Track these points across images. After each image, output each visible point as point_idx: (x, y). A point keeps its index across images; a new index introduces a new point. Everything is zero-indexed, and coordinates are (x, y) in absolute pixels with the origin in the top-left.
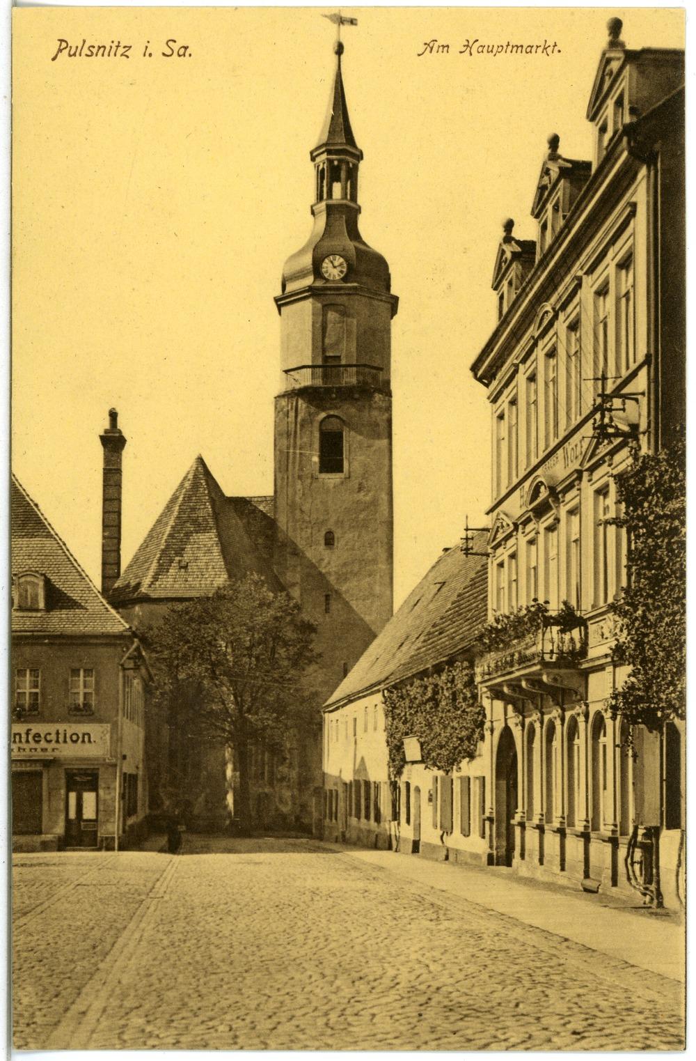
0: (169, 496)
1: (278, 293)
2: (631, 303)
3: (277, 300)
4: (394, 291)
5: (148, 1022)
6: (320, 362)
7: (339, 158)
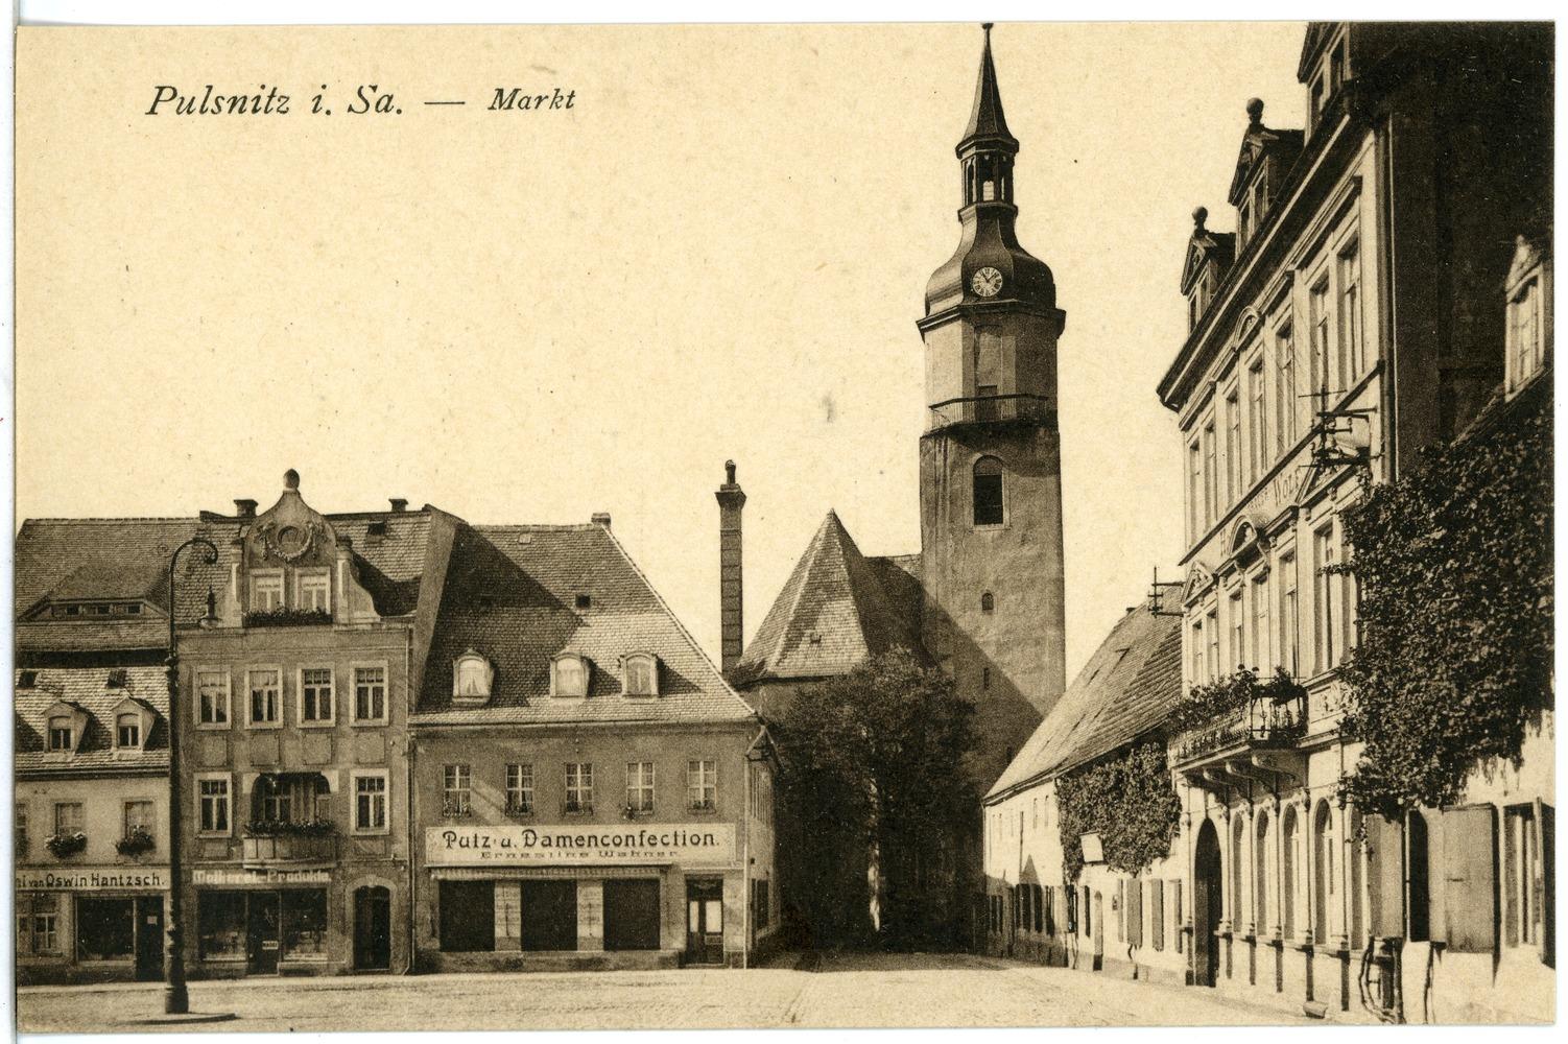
1: (922, 315)
3: (920, 324)
7: (991, 151)
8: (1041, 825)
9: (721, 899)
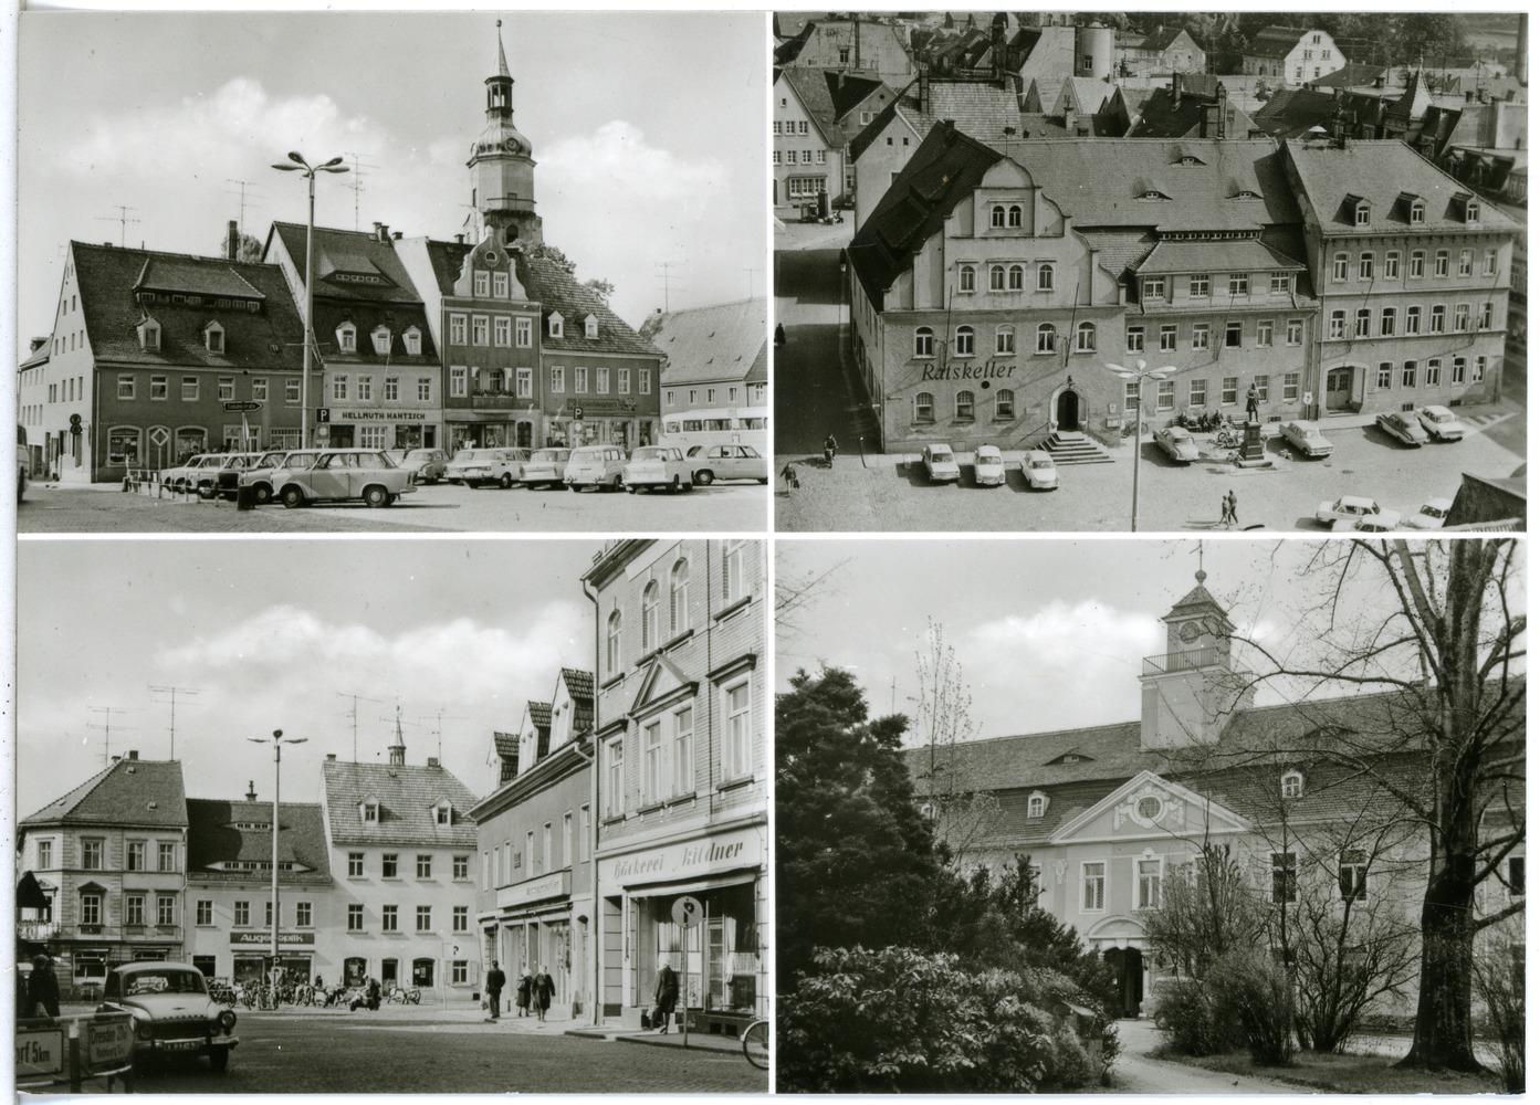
7: (251, 786)
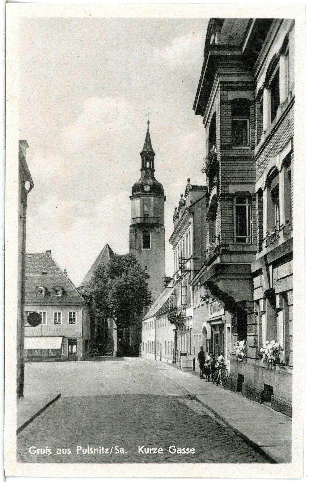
0: (102, 250)
1: (131, 195)
2: (188, 239)
3: (130, 197)
4: (165, 195)
5: (145, 418)
6: (143, 216)
7: (148, 155)
8: (162, 326)
9: (76, 345)
